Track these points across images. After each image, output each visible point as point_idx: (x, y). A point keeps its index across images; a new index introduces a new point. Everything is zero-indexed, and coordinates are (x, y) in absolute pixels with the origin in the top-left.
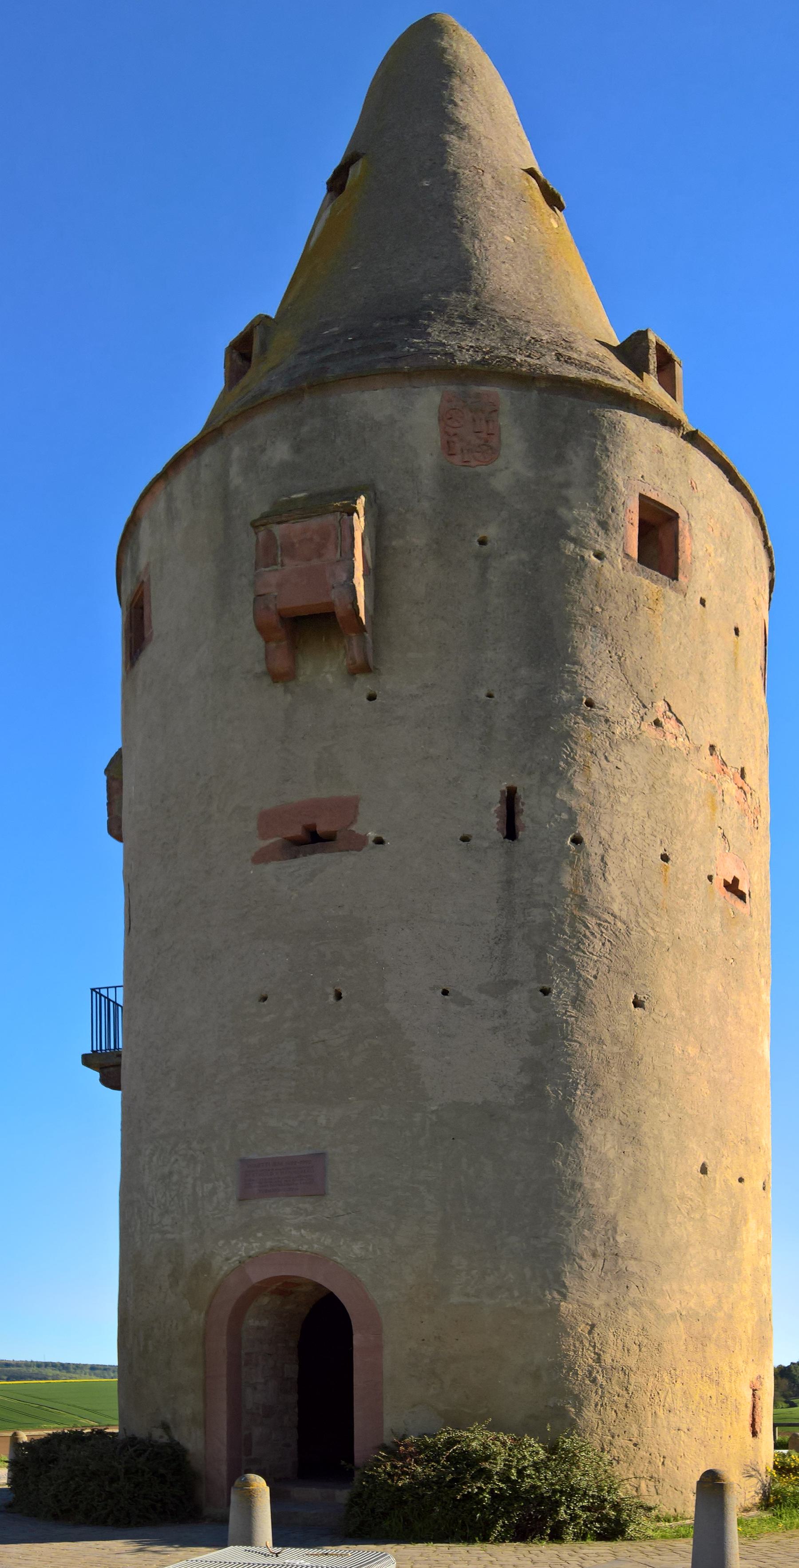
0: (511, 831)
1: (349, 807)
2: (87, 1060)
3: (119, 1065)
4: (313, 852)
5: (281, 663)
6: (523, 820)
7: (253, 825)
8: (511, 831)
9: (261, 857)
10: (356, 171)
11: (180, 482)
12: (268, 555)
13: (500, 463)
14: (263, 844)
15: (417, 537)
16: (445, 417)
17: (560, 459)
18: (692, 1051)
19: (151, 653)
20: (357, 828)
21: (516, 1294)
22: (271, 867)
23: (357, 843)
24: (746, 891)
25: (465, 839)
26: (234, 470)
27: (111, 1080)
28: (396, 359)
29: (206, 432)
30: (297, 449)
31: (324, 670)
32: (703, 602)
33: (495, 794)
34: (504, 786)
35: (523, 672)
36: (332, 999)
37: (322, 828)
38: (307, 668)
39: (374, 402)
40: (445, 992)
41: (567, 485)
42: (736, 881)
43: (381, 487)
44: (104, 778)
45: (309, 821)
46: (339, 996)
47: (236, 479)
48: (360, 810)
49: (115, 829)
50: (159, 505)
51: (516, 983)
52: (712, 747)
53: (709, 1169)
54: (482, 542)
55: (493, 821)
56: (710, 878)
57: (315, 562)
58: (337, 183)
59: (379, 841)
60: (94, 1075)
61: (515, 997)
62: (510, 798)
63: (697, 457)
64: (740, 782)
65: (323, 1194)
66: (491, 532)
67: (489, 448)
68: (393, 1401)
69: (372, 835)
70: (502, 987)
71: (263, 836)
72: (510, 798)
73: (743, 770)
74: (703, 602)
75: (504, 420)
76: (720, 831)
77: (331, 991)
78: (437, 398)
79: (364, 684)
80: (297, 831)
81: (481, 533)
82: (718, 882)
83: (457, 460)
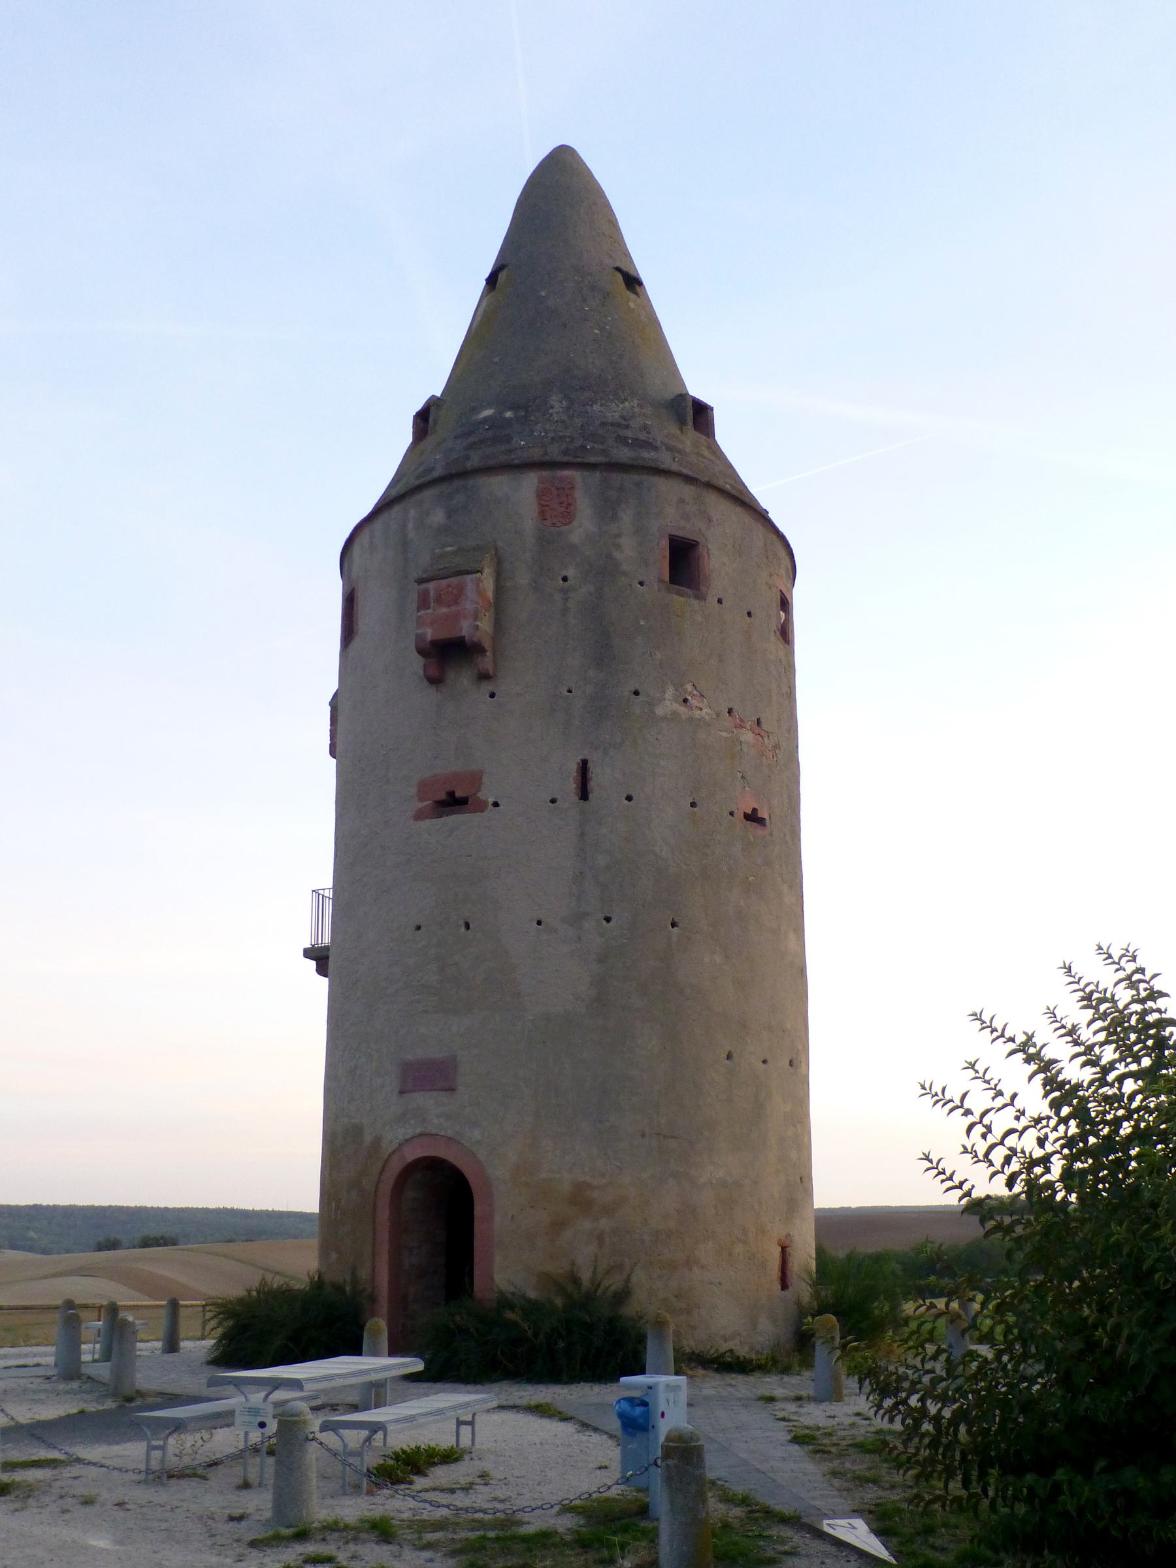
0: (584, 794)
1: (475, 779)
2: (308, 953)
3: (327, 958)
4: (453, 813)
5: (434, 672)
6: (592, 785)
7: (413, 791)
8: (584, 794)
9: (419, 816)
10: (502, 276)
11: (378, 525)
12: (423, 603)
13: (575, 523)
14: (421, 805)
15: (522, 578)
16: (541, 495)
17: (614, 517)
18: (718, 959)
19: (356, 643)
20: (481, 795)
21: (586, 1169)
22: (426, 824)
23: (481, 807)
24: (766, 816)
25: (553, 801)
26: (410, 525)
27: (322, 970)
28: (510, 451)
29: (394, 493)
30: (449, 516)
31: (462, 678)
32: (720, 601)
33: (573, 767)
34: (578, 760)
35: (592, 673)
36: (463, 929)
37: (459, 794)
38: (451, 675)
39: (498, 485)
40: (539, 923)
41: (619, 536)
42: (755, 810)
43: (500, 543)
44: (329, 708)
45: (449, 789)
46: (467, 927)
47: (411, 534)
48: (484, 780)
49: (333, 753)
50: (364, 538)
51: (587, 914)
52: (730, 711)
53: (735, 1055)
54: (565, 579)
55: (572, 786)
56: (732, 814)
57: (454, 608)
58: (492, 280)
59: (496, 804)
60: (312, 964)
61: (587, 925)
62: (584, 767)
63: (712, 498)
64: (757, 730)
65: (452, 1090)
66: (570, 572)
67: (568, 515)
68: (511, 1263)
69: (491, 800)
70: (576, 919)
71: (421, 800)
72: (584, 767)
73: (758, 720)
74: (720, 601)
75: (578, 493)
76: (739, 775)
77: (462, 922)
78: (536, 481)
79: (487, 687)
80: (442, 796)
81: (564, 573)
82: (739, 815)
83: (548, 522)
